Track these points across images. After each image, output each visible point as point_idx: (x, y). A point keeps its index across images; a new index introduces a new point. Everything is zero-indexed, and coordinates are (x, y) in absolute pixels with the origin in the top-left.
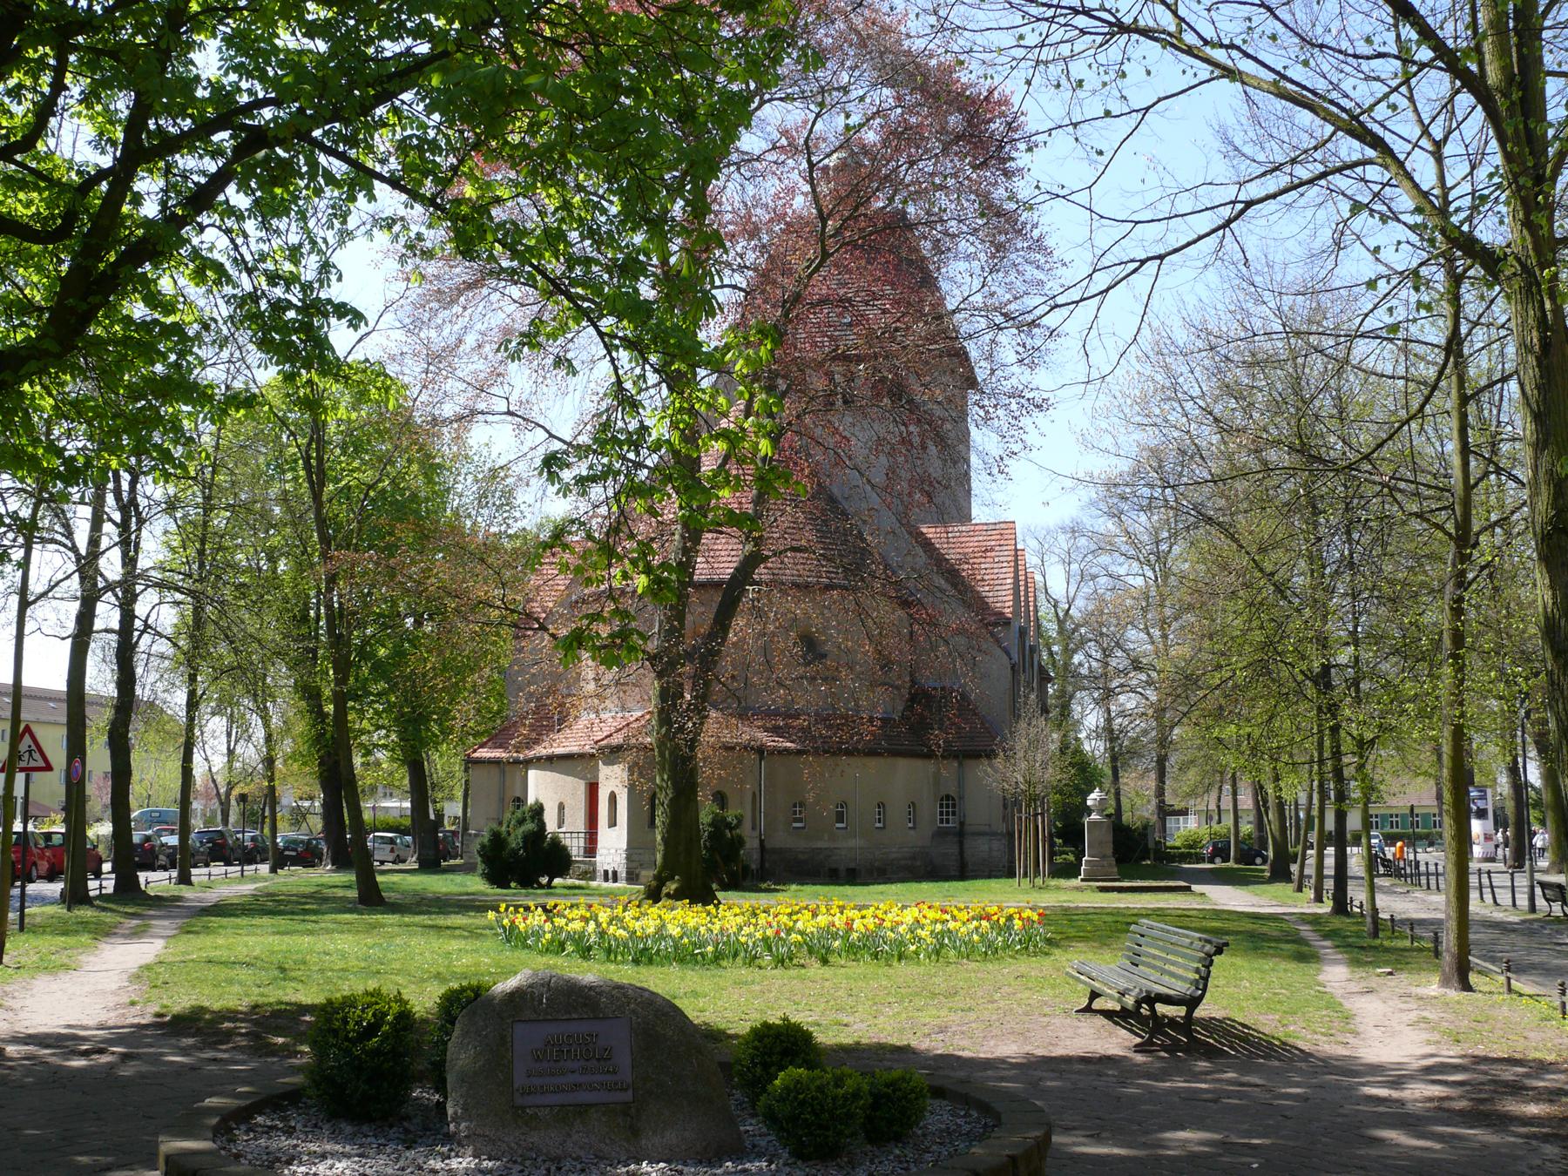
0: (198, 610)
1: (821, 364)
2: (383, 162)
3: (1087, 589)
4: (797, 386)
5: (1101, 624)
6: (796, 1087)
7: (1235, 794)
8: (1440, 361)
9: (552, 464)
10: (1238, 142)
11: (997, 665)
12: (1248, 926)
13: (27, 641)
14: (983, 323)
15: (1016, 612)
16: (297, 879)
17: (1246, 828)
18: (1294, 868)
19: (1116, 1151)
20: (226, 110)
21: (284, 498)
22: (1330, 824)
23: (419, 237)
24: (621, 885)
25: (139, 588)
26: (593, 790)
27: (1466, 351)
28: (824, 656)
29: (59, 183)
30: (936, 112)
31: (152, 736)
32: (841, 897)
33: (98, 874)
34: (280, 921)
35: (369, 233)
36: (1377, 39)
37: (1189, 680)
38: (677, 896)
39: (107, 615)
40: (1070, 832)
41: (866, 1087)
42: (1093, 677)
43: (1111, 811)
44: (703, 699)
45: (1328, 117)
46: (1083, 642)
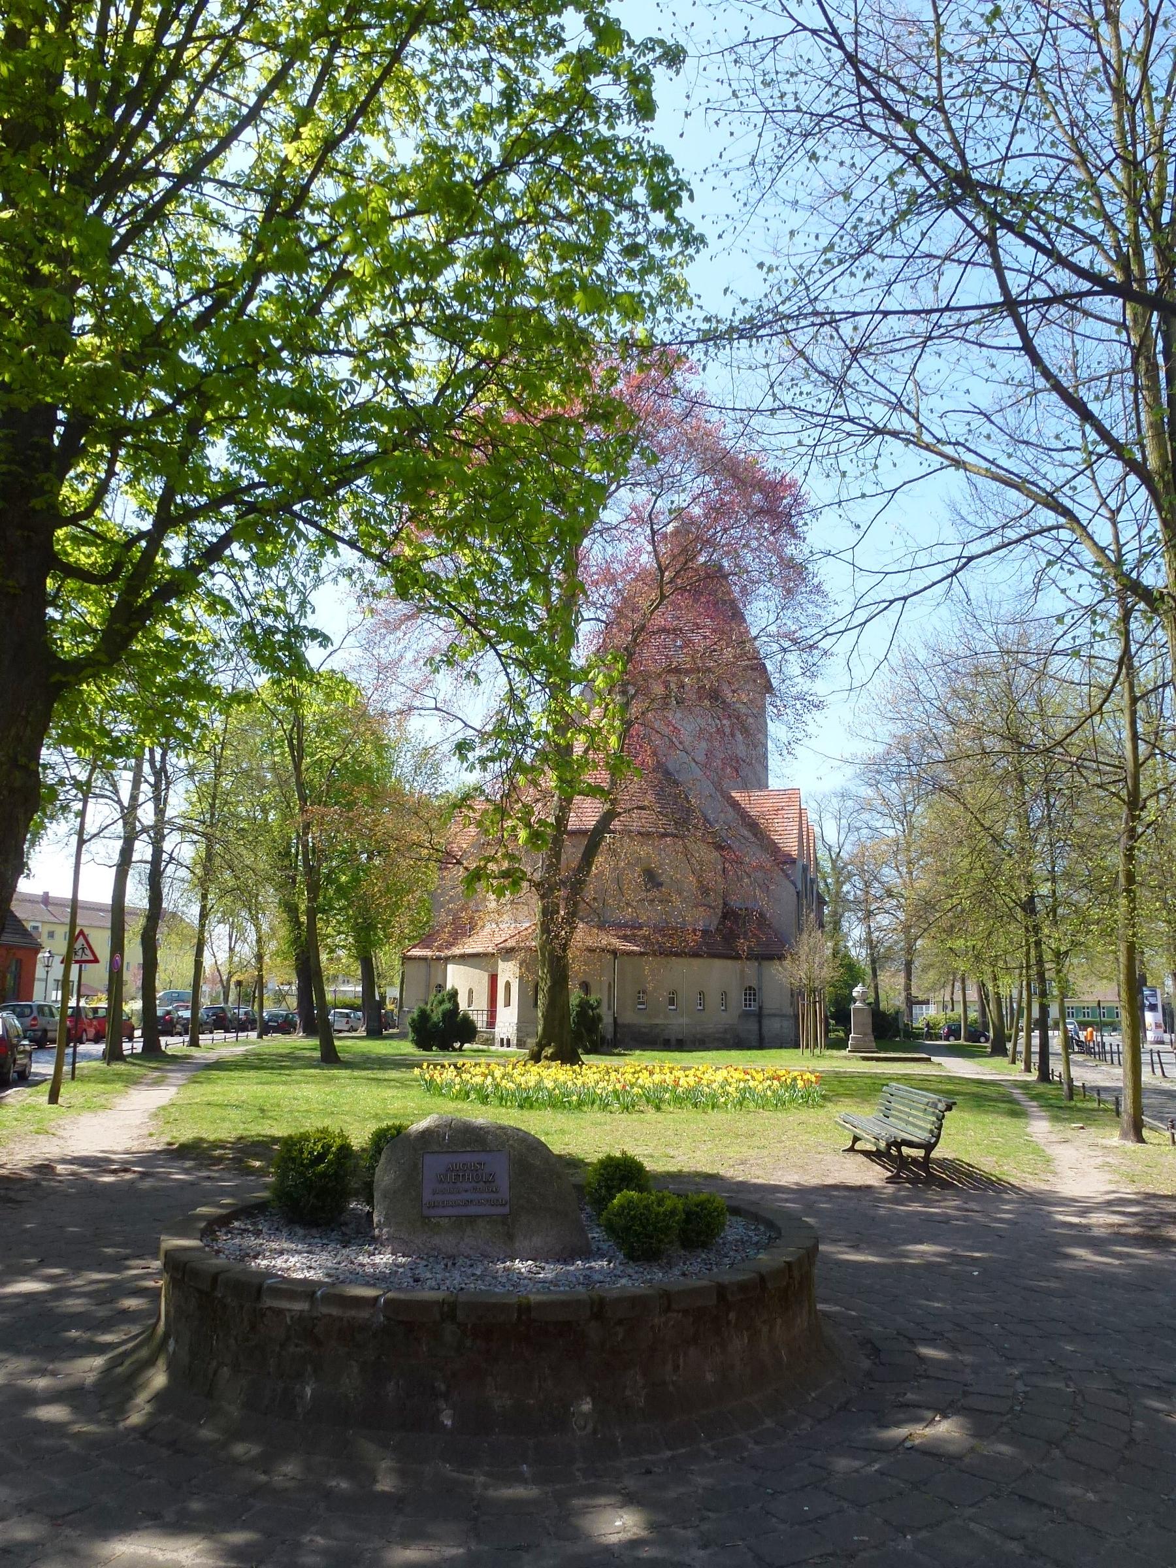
0: (209, 848)
1: (660, 675)
2: (344, 528)
3: (853, 838)
4: (643, 691)
5: (863, 863)
6: (629, 1204)
7: (964, 990)
8: (1115, 671)
9: (462, 748)
10: (964, 513)
11: (787, 893)
12: (975, 1089)
13: (82, 867)
14: (775, 647)
15: (801, 854)
16: (278, 1043)
17: (973, 1015)
18: (1009, 1046)
19: (871, 1258)
20: (232, 491)
21: (274, 767)
22: (1036, 1014)
23: (372, 583)
24: (513, 1049)
25: (166, 831)
26: (493, 979)
27: (1136, 664)
28: (661, 885)
29: (112, 541)
30: (743, 493)
31: (174, 938)
32: (670, 1061)
33: (131, 1038)
34: (263, 1075)
35: (335, 580)
36: (1064, 437)
37: (927, 905)
38: (552, 1058)
39: (143, 850)
40: (841, 1016)
41: (680, 1207)
42: (857, 901)
43: (871, 1000)
44: (572, 914)
45: (1029, 494)
46: (850, 875)
